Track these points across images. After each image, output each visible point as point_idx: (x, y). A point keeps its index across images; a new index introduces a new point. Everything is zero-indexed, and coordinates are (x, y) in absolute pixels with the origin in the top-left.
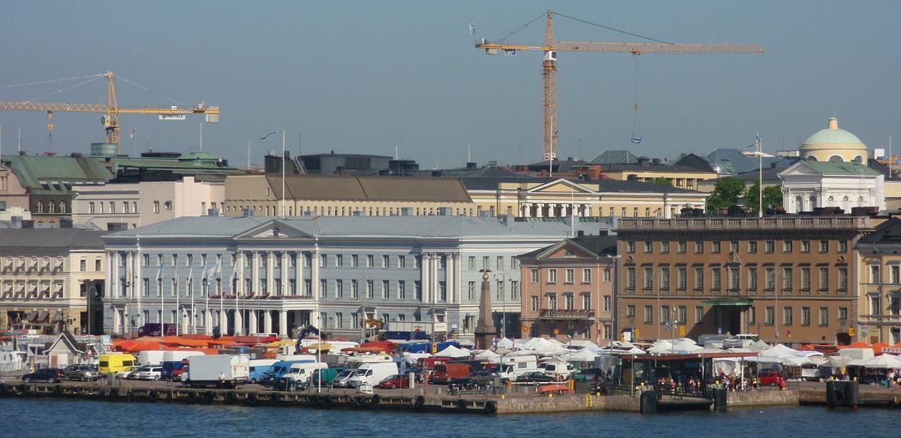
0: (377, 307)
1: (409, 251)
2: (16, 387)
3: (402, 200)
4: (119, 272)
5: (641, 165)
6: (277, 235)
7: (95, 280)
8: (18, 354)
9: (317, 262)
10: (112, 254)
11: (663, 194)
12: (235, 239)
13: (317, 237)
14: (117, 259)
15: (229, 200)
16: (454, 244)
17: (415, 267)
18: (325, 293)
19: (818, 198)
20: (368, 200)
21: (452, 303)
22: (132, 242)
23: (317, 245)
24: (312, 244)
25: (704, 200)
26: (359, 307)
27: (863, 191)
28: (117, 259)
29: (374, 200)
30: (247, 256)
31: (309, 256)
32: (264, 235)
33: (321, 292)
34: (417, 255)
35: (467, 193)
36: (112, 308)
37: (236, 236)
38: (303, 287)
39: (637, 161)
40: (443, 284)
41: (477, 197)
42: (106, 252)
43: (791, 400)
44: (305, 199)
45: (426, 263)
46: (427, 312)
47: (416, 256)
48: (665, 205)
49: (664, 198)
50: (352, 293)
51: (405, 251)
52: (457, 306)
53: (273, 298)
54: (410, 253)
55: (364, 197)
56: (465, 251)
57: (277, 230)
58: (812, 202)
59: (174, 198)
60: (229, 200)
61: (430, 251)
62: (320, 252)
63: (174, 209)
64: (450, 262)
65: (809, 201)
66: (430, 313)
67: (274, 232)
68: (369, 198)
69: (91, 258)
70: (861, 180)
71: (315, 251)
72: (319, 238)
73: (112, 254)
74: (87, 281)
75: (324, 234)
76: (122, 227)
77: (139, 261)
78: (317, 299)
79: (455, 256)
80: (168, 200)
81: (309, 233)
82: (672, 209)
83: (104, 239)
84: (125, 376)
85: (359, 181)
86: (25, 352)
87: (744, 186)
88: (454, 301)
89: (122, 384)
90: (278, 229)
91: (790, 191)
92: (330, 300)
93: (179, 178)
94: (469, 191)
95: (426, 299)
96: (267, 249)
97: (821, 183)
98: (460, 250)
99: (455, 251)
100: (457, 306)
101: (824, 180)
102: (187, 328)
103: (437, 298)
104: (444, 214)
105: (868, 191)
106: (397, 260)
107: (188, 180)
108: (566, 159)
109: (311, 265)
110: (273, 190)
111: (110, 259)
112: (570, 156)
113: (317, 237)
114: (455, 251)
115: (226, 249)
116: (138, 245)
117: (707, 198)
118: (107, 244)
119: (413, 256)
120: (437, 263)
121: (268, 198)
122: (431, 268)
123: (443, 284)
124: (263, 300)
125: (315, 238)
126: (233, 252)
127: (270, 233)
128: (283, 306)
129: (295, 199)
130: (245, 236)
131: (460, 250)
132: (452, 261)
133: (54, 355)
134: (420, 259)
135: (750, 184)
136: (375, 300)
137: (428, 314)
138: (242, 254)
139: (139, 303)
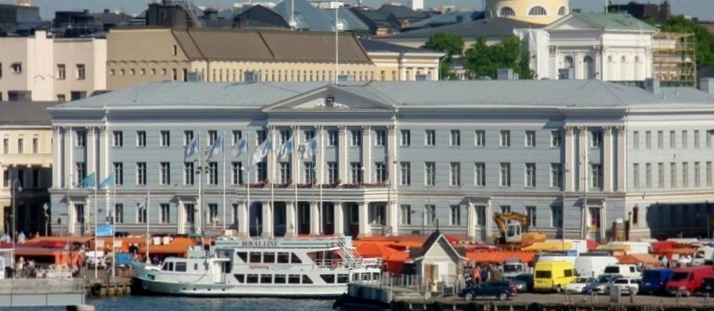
0: (492, 198)
1: (543, 124)
2: (427, 305)
3: (245, 60)
4: (74, 155)
5: (209, 19)
6: (332, 105)
7: (19, 166)
8: (215, 262)
9: (395, 140)
10: (63, 131)
11: (398, 54)
12: (265, 110)
13: (397, 107)
14: (71, 137)
15: (114, 62)
16: (619, 115)
17: (552, 145)
18: (407, 180)
19: (598, 59)
20: (277, 61)
21: (612, 190)
22: (98, 115)
23: (395, 117)
24: (388, 117)
25: (437, 61)
26: (577, 199)
27: (639, 50)
28: (72, 139)
29: (283, 61)
30: (283, 133)
31: (382, 134)
32: (310, 105)
33: (401, 179)
34: (556, 130)
35: (366, 56)
36: (65, 201)
37: (265, 107)
38: (325, 172)
39: (203, 14)
40: (599, 169)
41: (381, 60)
42: (54, 129)
43: (379, 291)
44: (218, 59)
45: (570, 140)
46: (60, 199)
47: (553, 132)
48: (400, 68)
49: (399, 59)
50: (451, 180)
51: (241, 125)
52: (622, 196)
53: (346, 186)
54: (545, 128)
55: (270, 57)
56: (631, 124)
57: (330, 99)
58: (586, 64)
59: (25, 57)
60: (114, 62)
61: (579, 124)
62: (110, 127)
63: (26, 72)
64: (609, 140)
65: (583, 63)
66: (580, 204)
67: (327, 102)
68: (276, 58)
69: (28, 136)
70: (640, 37)
71: (105, 127)
72: (399, 109)
73: (63, 131)
74: (11, 167)
75: (405, 104)
76: (81, 95)
77: (107, 140)
78: (396, 188)
79: (616, 131)
80: (17, 60)
81: (386, 102)
82: (407, 72)
83: (52, 112)
84: (580, 290)
85: (261, 36)
86: (228, 259)
87: (462, 43)
88: (63, 185)
89: (634, 300)
90: (333, 98)
91: (557, 50)
92: (441, 189)
93: (31, 33)
94: (369, 54)
95: (570, 186)
96: (315, 124)
97: (601, 40)
98: (625, 124)
99: (617, 124)
100: (622, 196)
101: (605, 37)
102: (184, 226)
103: (587, 186)
104: (567, 78)
105: (643, 50)
106: (523, 137)
107: (40, 35)
108: (103, 11)
109: (336, 143)
110: (182, 47)
111: (59, 137)
112: (106, 8)
113: (397, 107)
114: (617, 124)
115: (247, 124)
116: (105, 119)
117: (441, 58)
118: (55, 118)
119: (549, 132)
120: (587, 140)
121: (175, 58)
122: (579, 148)
123: (599, 169)
124: (307, 189)
125: (395, 108)
126: (260, 128)
127: (321, 102)
128: (365, 196)
129: (207, 60)
130: (275, 108)
131: (625, 124)
132: (611, 138)
133: (429, 263)
134: (560, 139)
135: (471, 40)
136: (489, 188)
137: (575, 205)
138: (586, 131)
139: (107, 195)
